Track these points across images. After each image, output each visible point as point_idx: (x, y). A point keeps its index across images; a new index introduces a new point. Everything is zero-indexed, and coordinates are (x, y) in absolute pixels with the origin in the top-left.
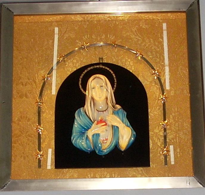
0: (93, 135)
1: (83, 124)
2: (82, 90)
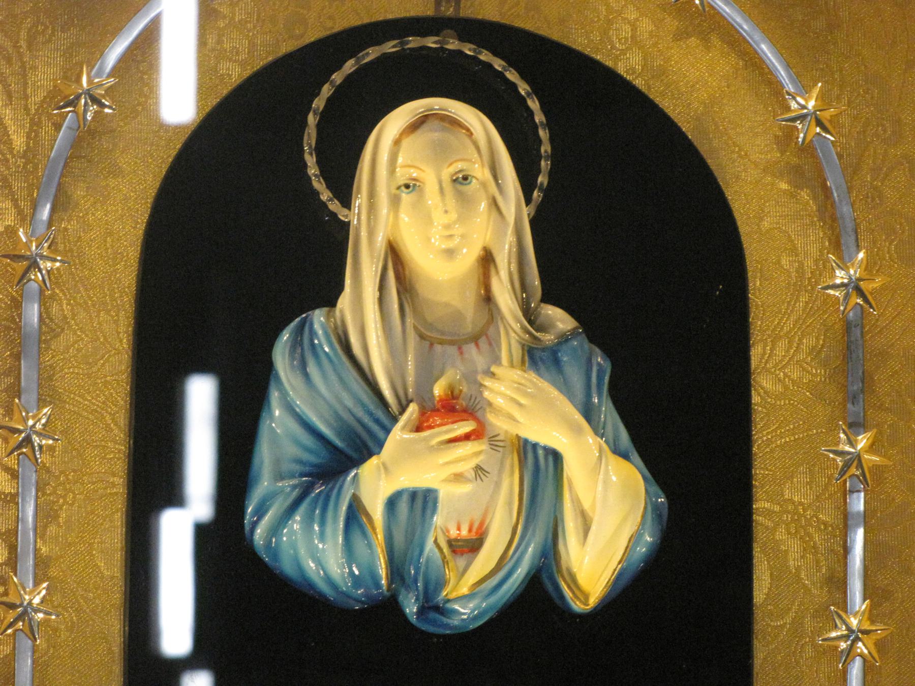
0: (392, 503)
2: (335, 206)
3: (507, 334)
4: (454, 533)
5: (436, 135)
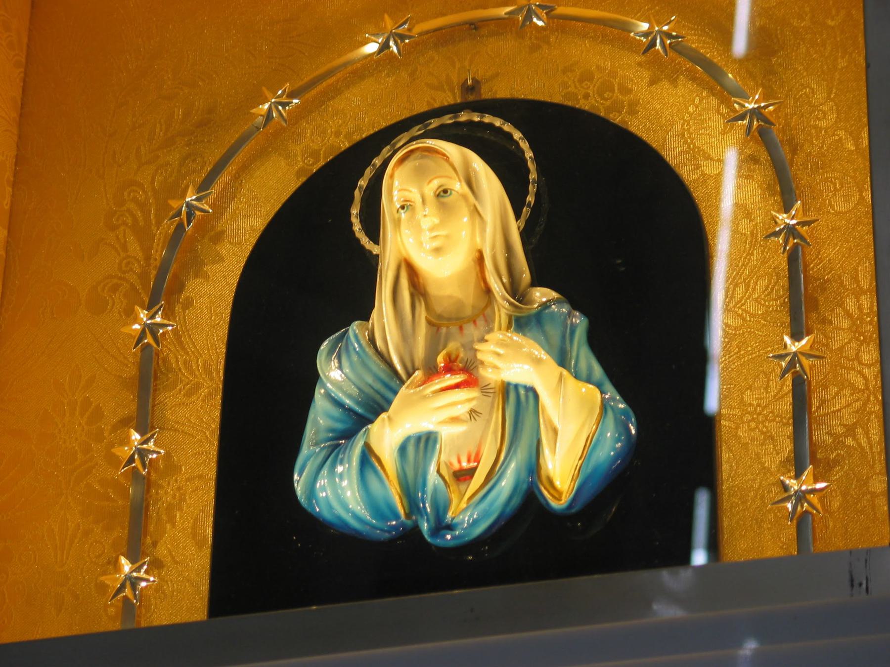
0: (403, 449)
1: (350, 396)
2: (365, 241)
5: (417, 163)
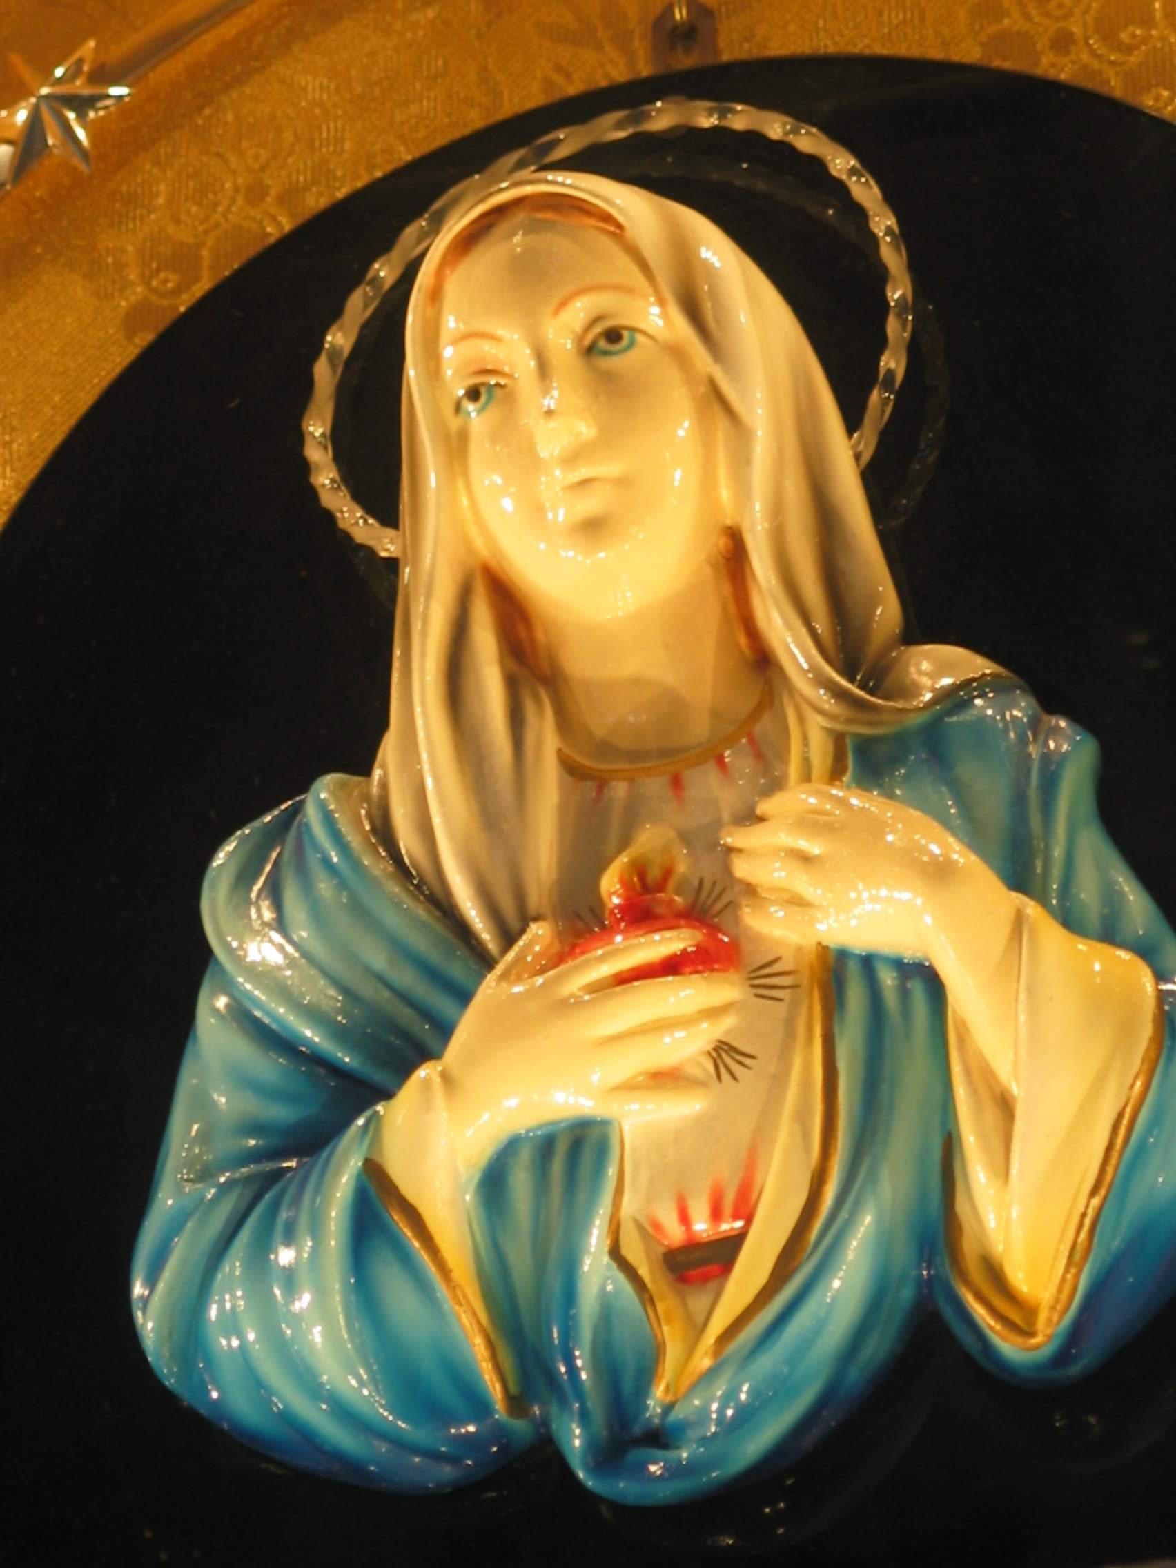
3: (802, 721)
4: (675, 1233)
